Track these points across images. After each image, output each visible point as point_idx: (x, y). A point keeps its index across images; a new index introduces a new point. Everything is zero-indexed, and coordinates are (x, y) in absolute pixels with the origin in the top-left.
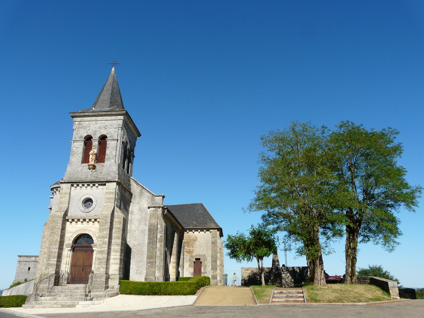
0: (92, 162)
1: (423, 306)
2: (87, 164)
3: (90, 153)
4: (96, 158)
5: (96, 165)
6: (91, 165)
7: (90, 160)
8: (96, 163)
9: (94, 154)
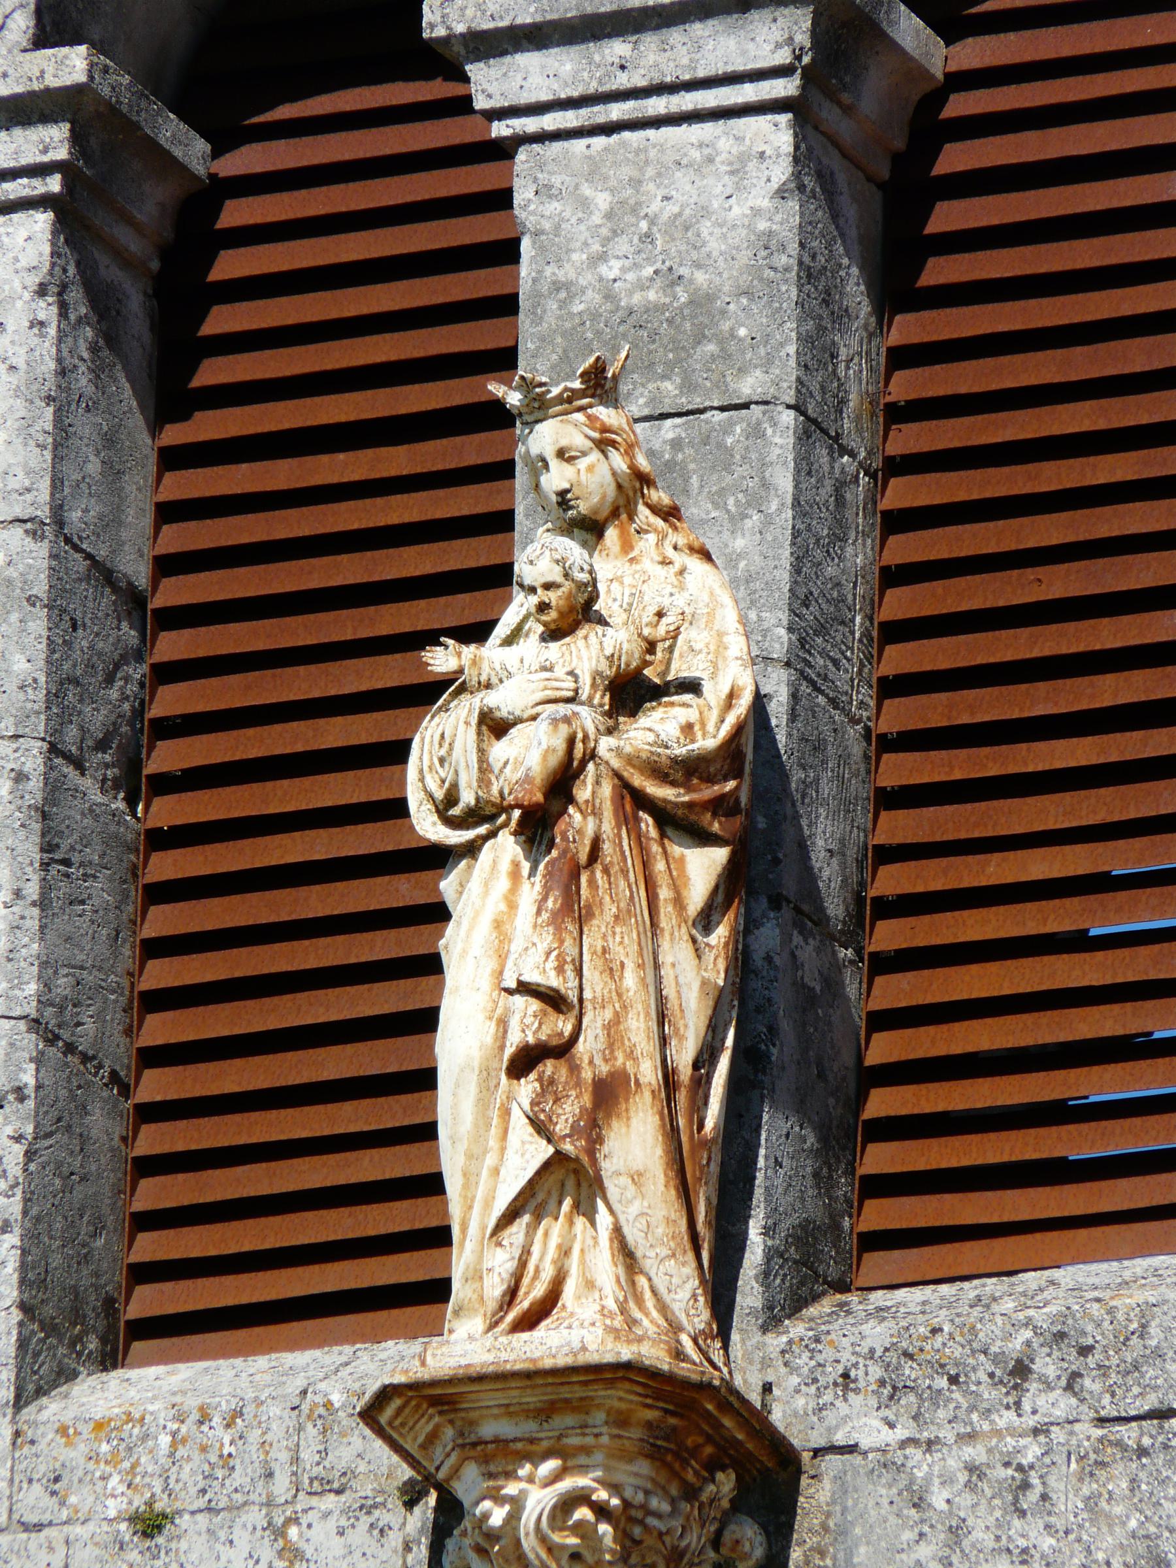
0: (569, 1257)
1: (2, 738)
2: (353, 1366)
3: (440, 755)
4: (774, 1036)
5: (785, 1372)
6: (559, 1401)
7: (484, 1144)
8: (817, 1271)
9: (667, 807)
